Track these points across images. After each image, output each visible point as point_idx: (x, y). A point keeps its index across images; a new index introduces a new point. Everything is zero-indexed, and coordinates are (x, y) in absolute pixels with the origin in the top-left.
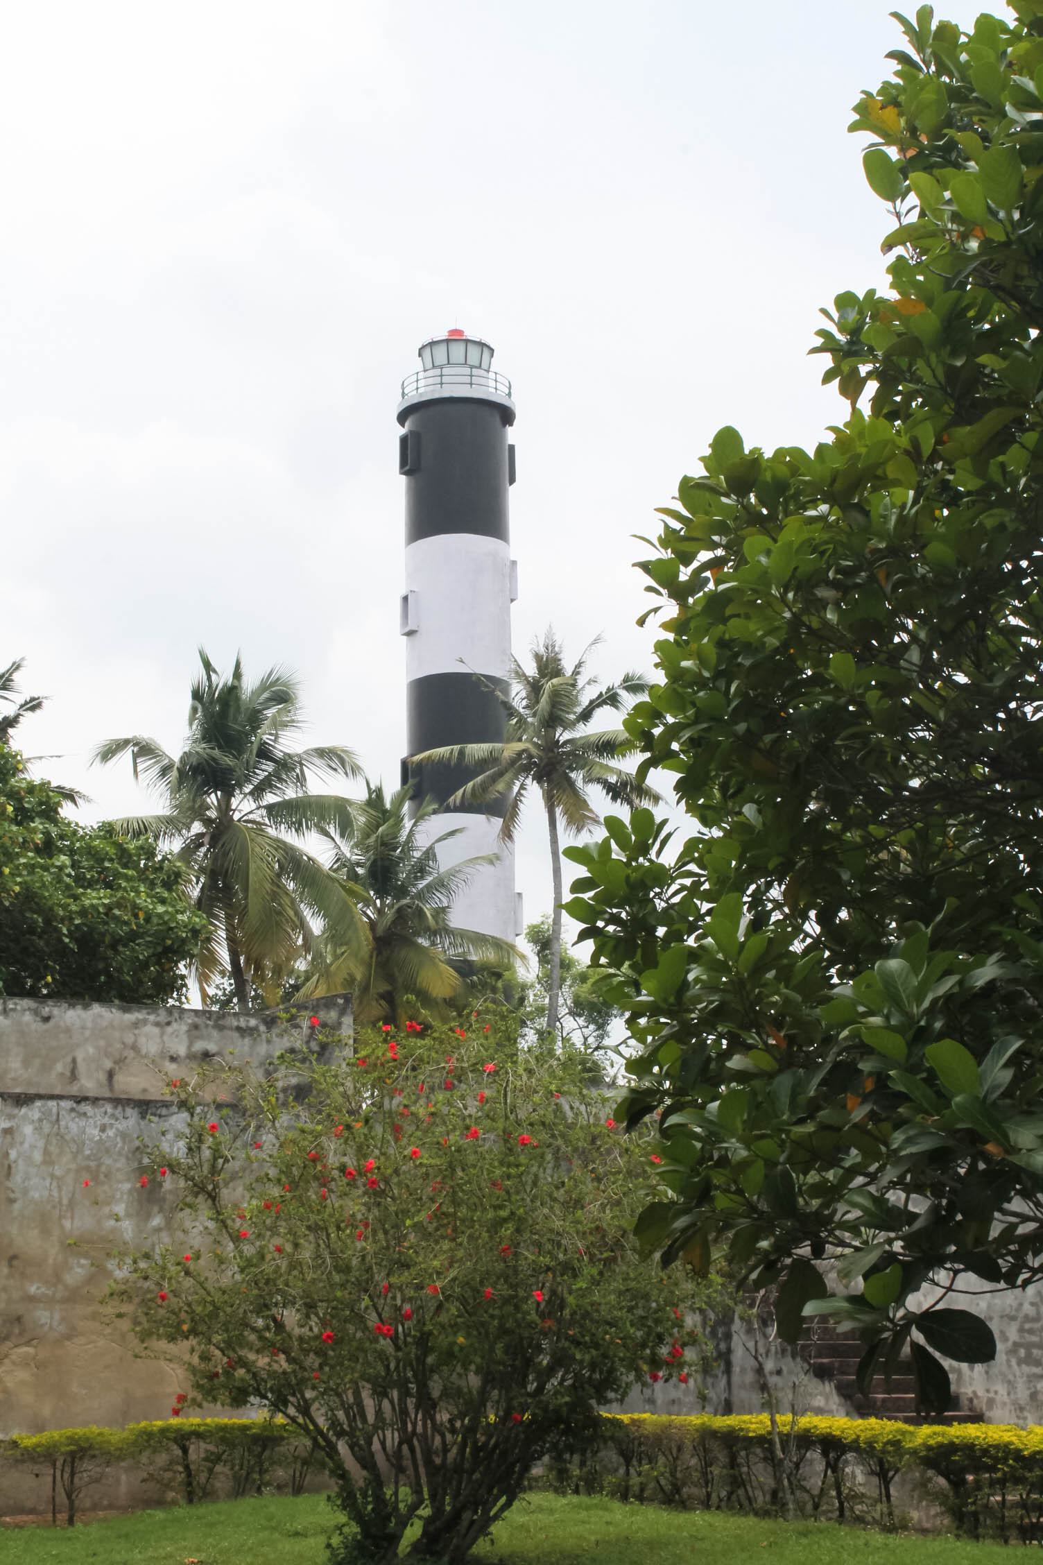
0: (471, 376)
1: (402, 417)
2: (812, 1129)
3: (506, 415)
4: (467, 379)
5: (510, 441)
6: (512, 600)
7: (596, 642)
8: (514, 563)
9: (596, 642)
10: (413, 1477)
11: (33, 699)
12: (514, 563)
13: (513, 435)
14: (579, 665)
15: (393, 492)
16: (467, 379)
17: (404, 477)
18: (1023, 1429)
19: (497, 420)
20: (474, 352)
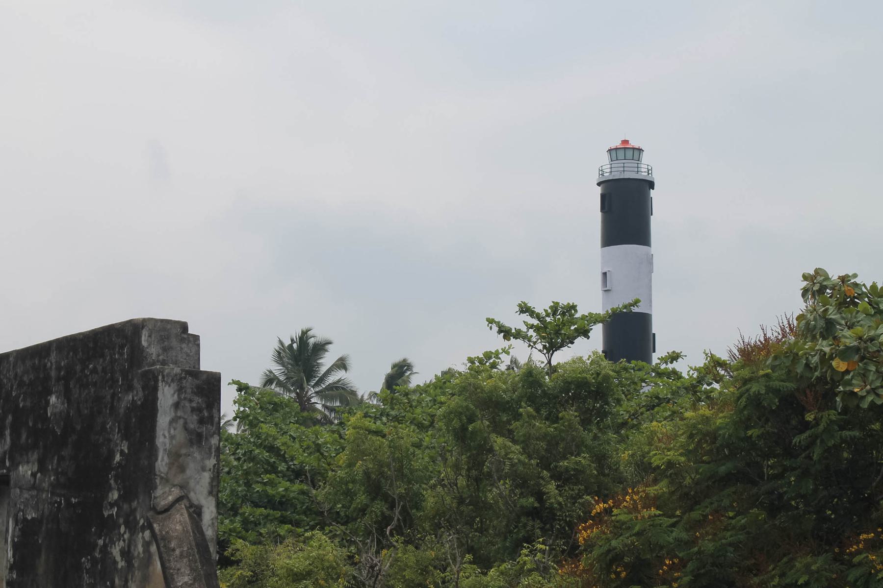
3: (651, 185)
13: (653, 193)
20: (629, 153)
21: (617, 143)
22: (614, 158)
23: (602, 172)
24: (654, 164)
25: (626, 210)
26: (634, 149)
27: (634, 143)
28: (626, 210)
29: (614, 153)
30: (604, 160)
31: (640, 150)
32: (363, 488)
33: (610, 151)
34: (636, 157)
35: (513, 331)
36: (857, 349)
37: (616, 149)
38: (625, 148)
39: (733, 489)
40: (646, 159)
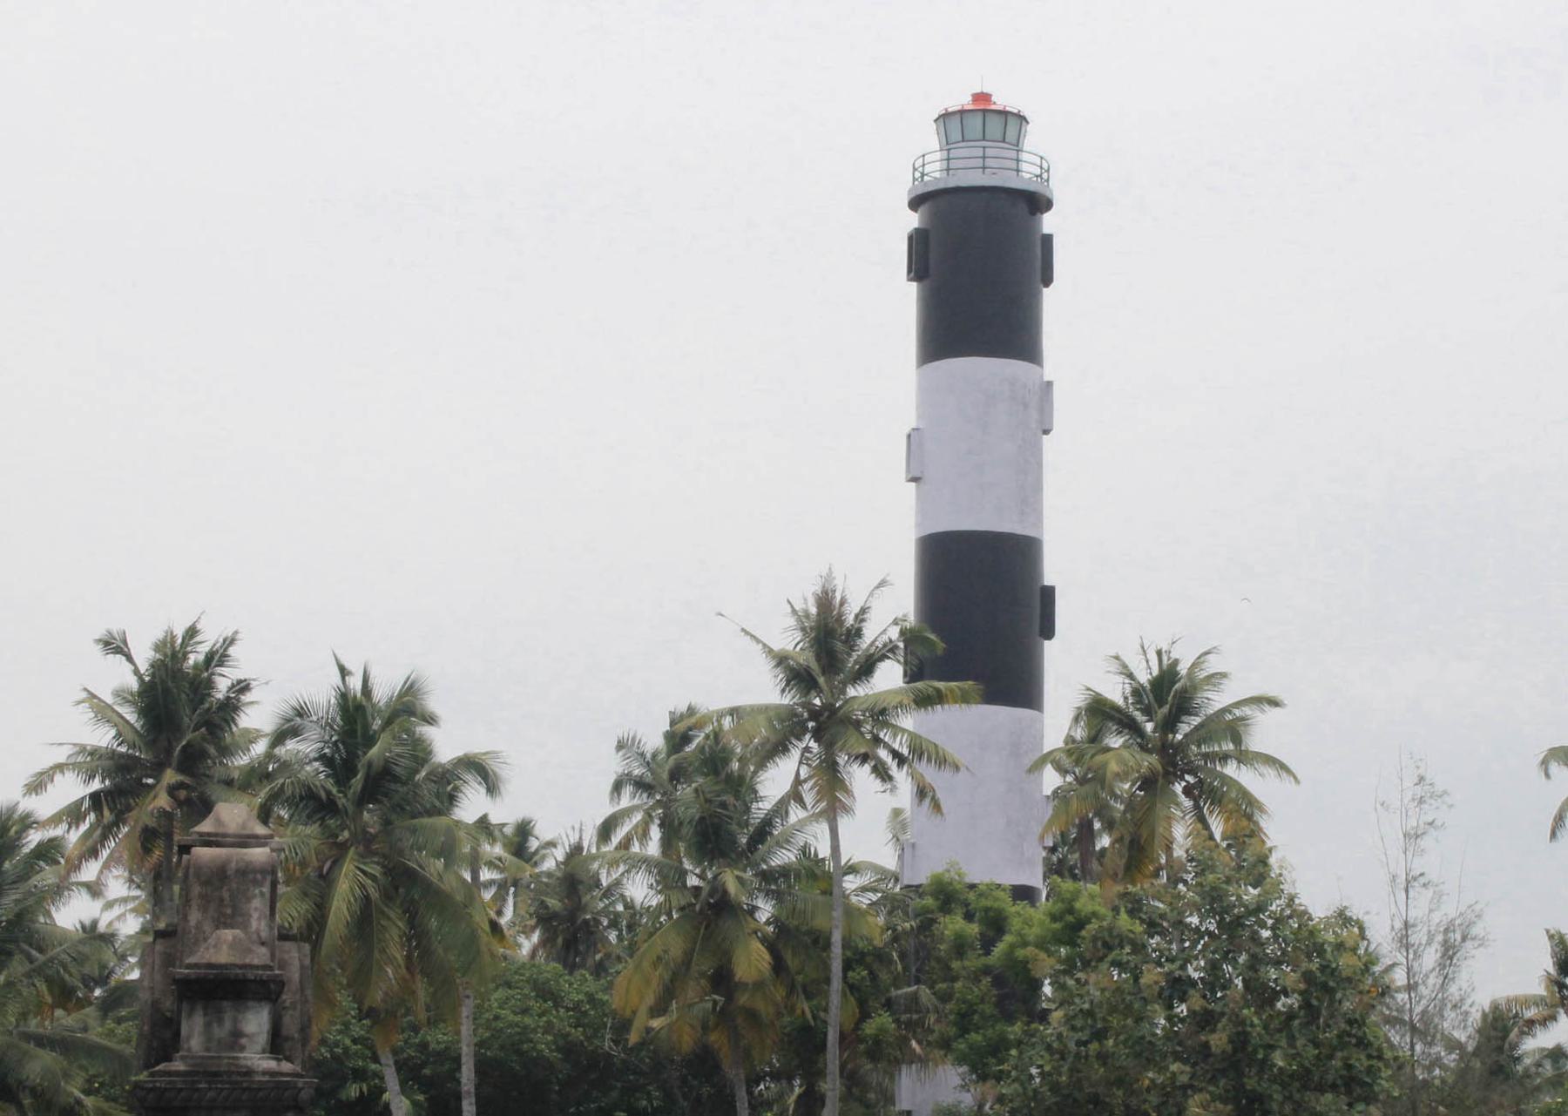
0: (984, 157)
1: (915, 203)
2: (7, 865)
3: (1037, 203)
4: (979, 162)
5: (1046, 230)
6: (1046, 432)
7: (882, 583)
8: (1050, 384)
9: (882, 583)
10: (268, 895)
11: (239, 682)
12: (1050, 384)
13: (1049, 223)
14: (863, 611)
15: (900, 304)
16: (979, 162)
17: (914, 284)
18: (1126, 1040)
19: (1022, 208)
20: (994, 125)
21: (963, 100)
22: (956, 135)
23: (919, 173)
24: (1050, 153)
25: (979, 266)
26: (1004, 114)
27: (1001, 101)
28: (979, 266)
29: (955, 124)
30: (930, 140)
31: (1021, 119)
32: (735, 765)
33: (945, 117)
34: (1011, 134)
35: (1079, 734)
36: (1217, 978)
37: (962, 112)
38: (985, 111)
39: (549, 865)
40: (1033, 140)
